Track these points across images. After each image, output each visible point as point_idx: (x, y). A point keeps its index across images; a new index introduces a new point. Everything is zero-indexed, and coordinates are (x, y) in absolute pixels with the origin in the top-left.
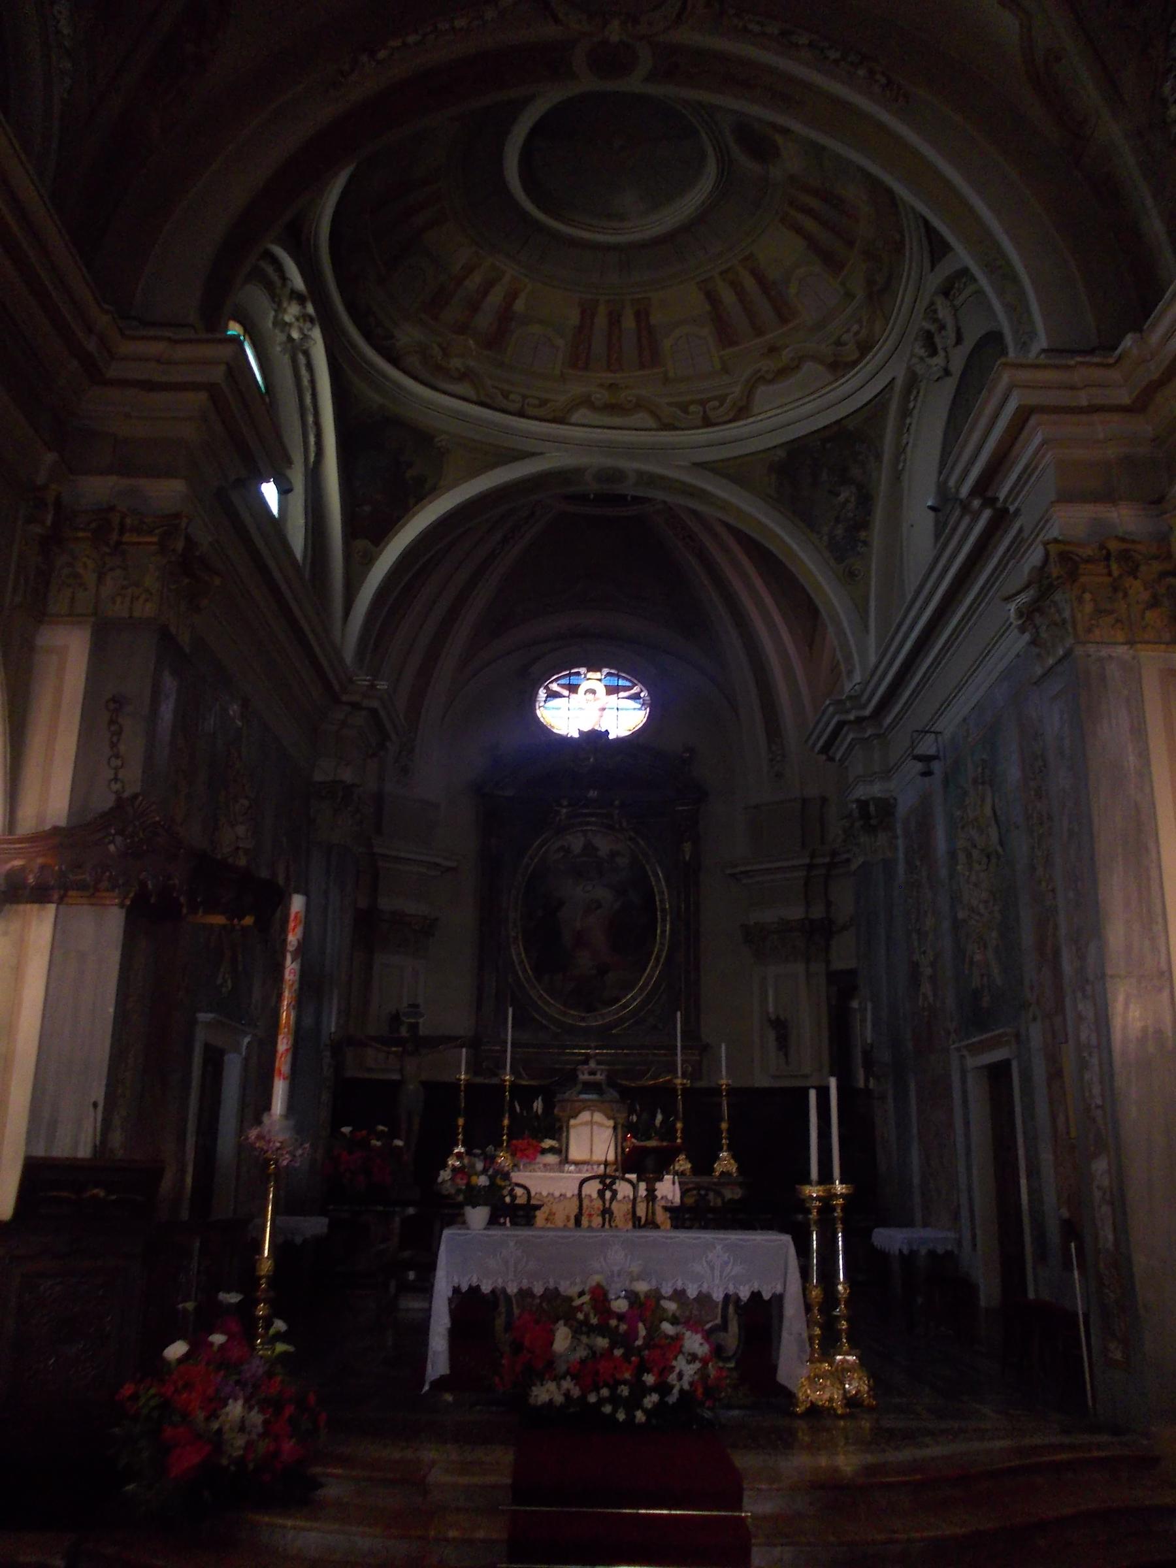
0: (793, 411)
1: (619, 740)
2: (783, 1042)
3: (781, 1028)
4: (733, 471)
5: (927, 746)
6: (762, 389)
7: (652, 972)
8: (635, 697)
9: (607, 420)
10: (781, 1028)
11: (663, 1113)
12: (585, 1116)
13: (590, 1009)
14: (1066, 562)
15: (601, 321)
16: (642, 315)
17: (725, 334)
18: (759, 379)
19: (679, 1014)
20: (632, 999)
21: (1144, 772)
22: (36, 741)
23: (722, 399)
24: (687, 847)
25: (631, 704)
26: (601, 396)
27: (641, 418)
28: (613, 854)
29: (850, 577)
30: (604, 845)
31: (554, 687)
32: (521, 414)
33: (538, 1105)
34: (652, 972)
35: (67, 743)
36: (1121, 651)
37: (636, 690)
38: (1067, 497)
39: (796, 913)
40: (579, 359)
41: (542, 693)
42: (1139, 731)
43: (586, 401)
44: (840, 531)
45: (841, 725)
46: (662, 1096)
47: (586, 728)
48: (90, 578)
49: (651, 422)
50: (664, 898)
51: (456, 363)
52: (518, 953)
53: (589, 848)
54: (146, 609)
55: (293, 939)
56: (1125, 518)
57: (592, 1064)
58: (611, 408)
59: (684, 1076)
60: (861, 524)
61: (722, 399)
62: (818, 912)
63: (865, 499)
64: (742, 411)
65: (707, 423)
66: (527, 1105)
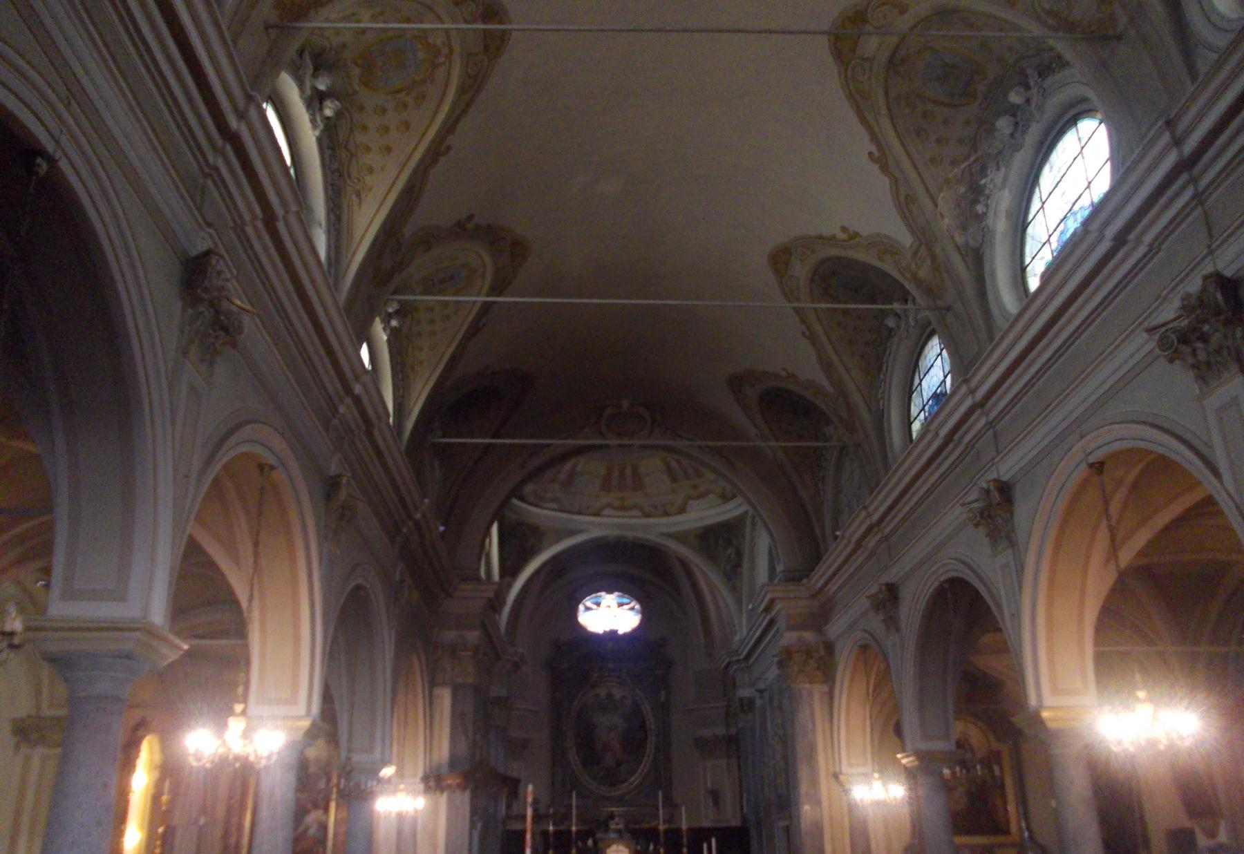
0: (704, 513)
1: (625, 635)
2: (716, 802)
3: (715, 796)
4: (680, 537)
5: (761, 685)
6: (691, 502)
7: (646, 765)
8: (632, 609)
9: (621, 513)
10: (715, 796)
11: (951, 344)
12: (614, 847)
13: (612, 785)
14: (788, 653)
15: (616, 473)
16: (635, 470)
17: (674, 479)
18: (690, 497)
19: (660, 793)
20: (635, 779)
21: (814, 729)
22: (436, 727)
23: (672, 504)
24: (663, 693)
25: (632, 613)
26: (616, 503)
27: (636, 512)
28: (624, 697)
29: (734, 589)
30: (618, 693)
31: (589, 604)
32: (579, 513)
33: (590, 842)
34: (646, 765)
35: (446, 730)
36: (807, 686)
37: (632, 604)
38: (790, 628)
39: (721, 731)
40: (606, 486)
41: (581, 607)
42: (813, 715)
43: (609, 505)
44: (728, 567)
45: (729, 663)
46: (651, 835)
47: (608, 629)
48: (449, 669)
49: (640, 514)
50: (651, 722)
51: (549, 495)
52: (573, 755)
53: (610, 695)
54: (470, 680)
55: (530, 800)
56: (809, 636)
57: (617, 819)
58: (622, 508)
59: (665, 822)
60: (738, 565)
61: (672, 504)
62: (733, 731)
63: (739, 554)
64: (682, 510)
65: (666, 514)
66: (585, 842)
